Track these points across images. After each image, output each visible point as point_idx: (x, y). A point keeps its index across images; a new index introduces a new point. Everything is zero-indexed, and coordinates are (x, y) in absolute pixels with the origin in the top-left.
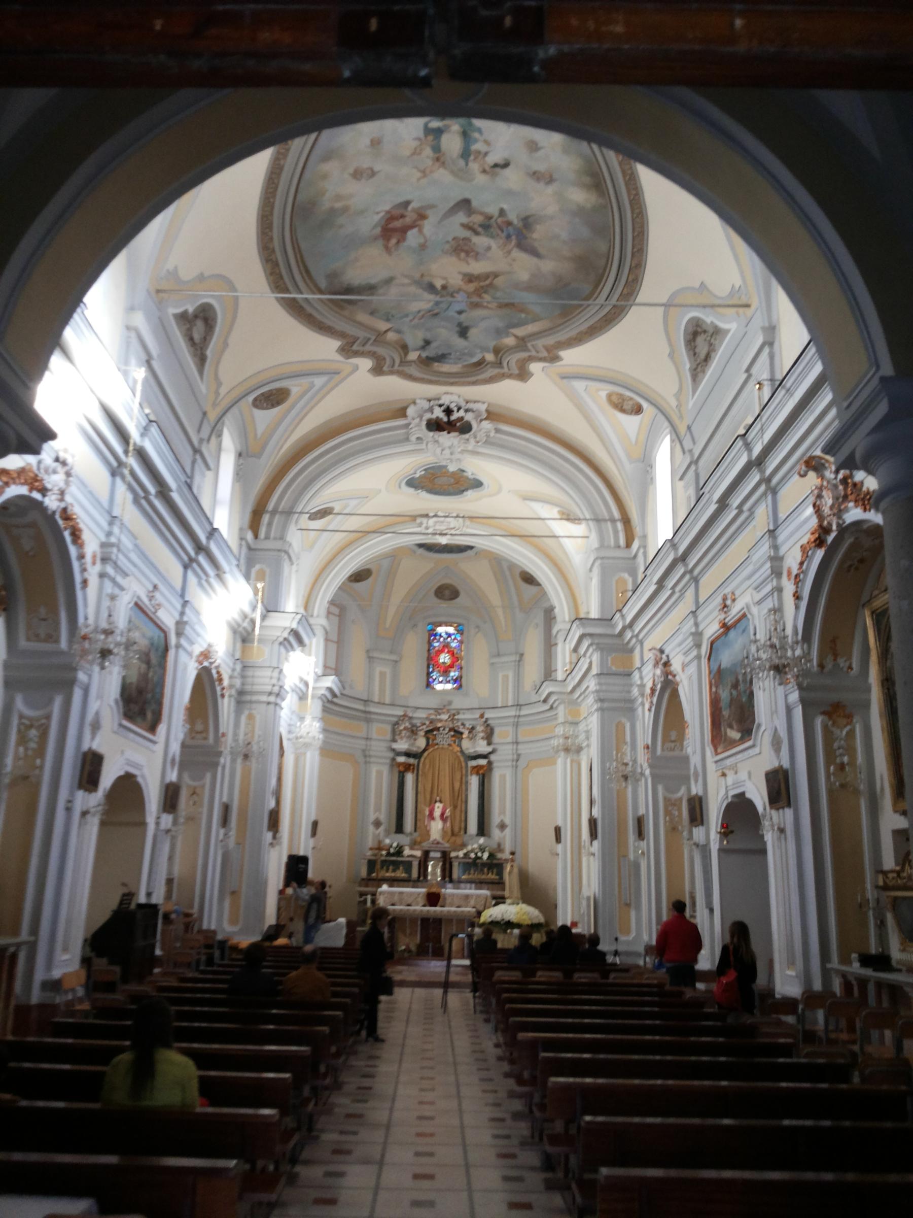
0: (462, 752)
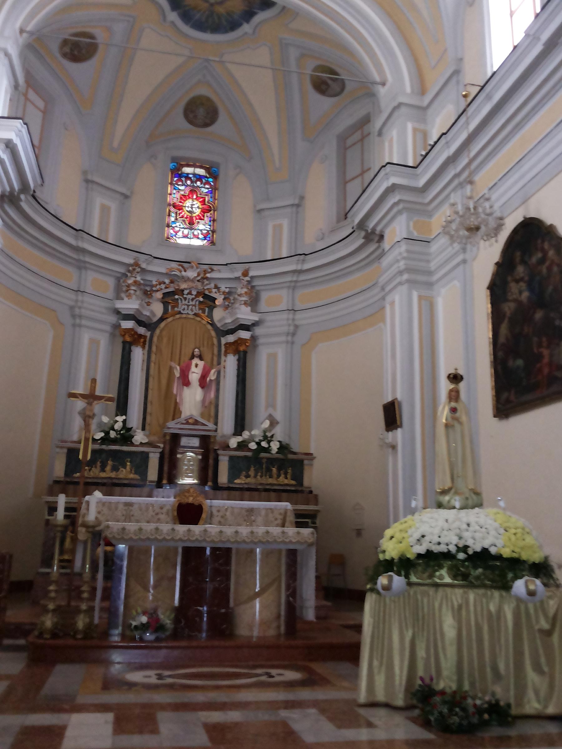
0: (213, 324)
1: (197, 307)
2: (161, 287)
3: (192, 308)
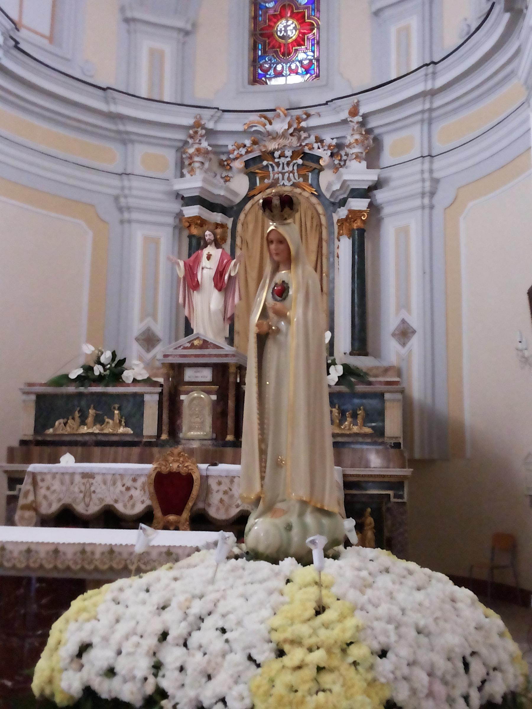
1: (296, 174)
2: (241, 152)
3: (289, 176)
